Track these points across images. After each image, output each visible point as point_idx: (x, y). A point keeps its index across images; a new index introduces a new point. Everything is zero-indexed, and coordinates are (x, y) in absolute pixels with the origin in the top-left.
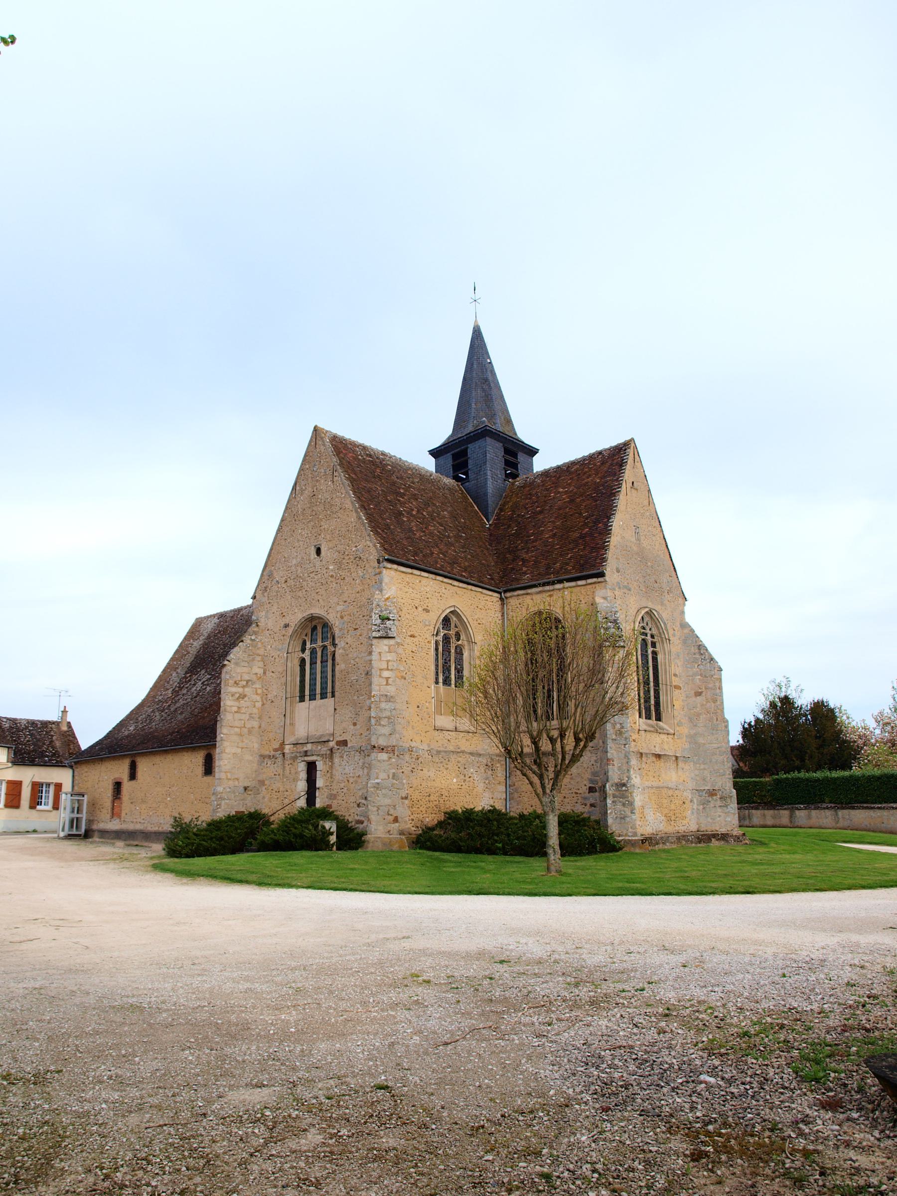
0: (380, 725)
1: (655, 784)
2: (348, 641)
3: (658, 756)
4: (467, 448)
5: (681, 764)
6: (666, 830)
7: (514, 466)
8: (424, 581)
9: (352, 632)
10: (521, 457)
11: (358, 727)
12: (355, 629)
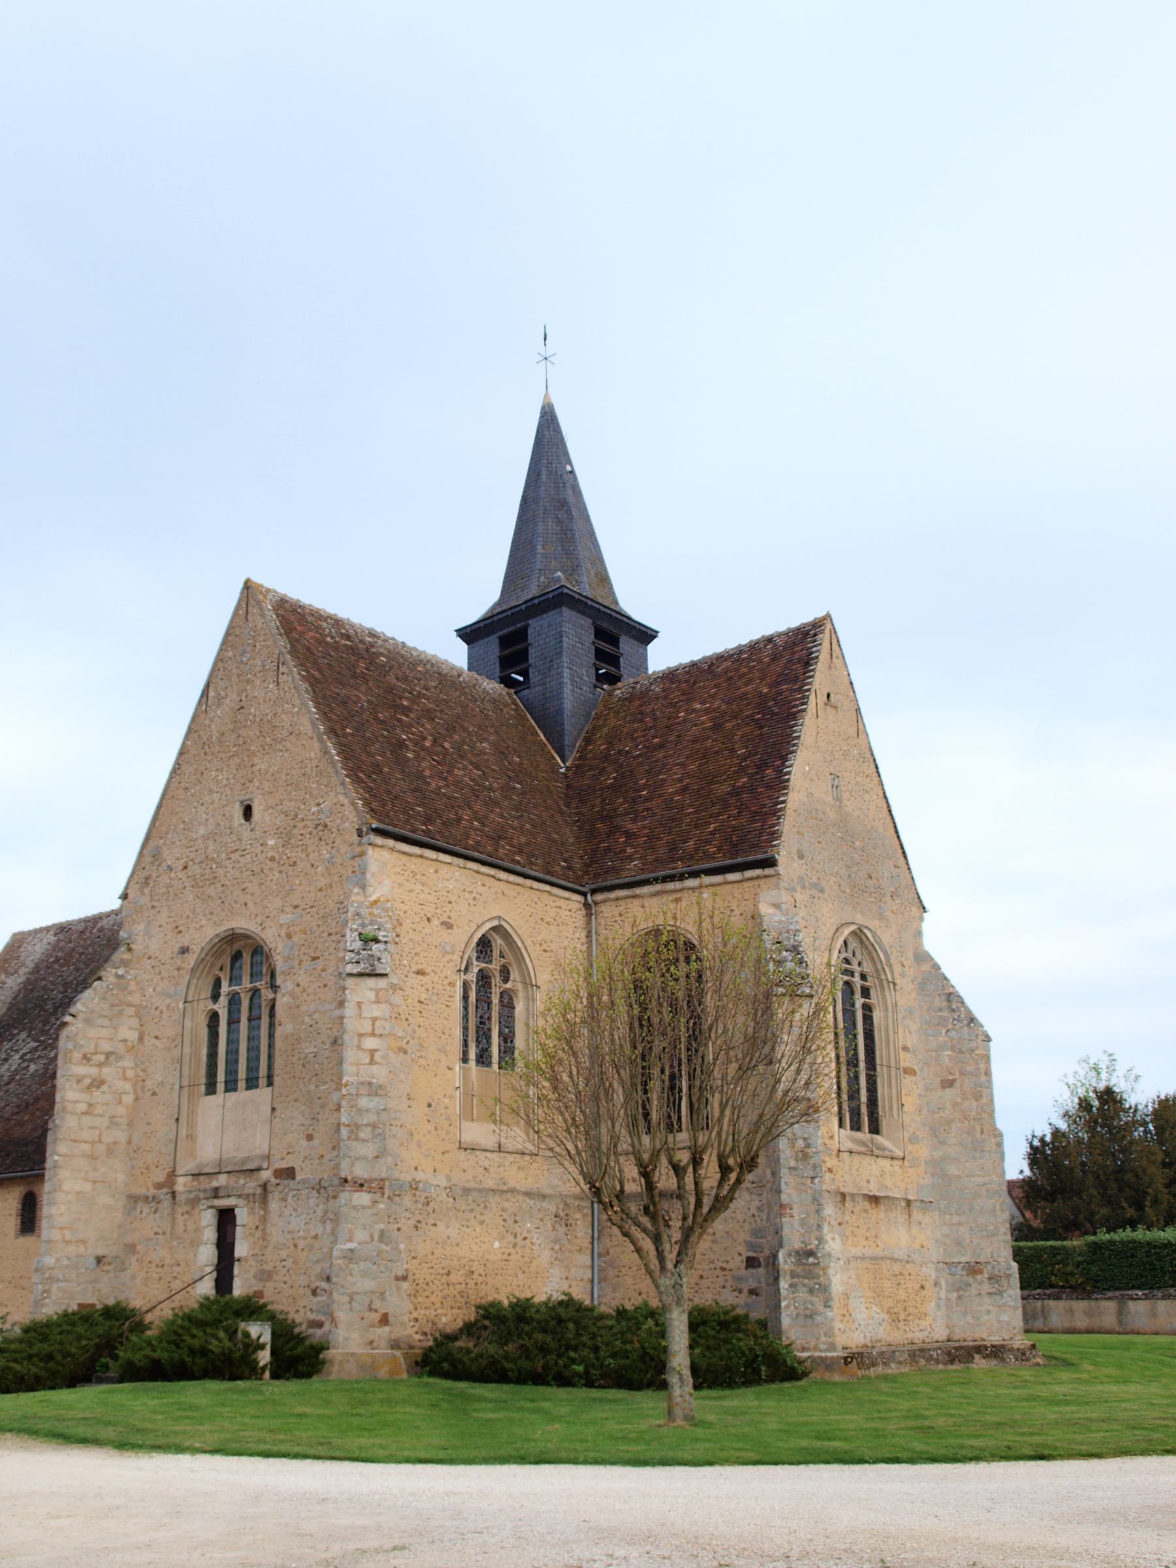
0: (357, 1139)
1: (868, 1252)
3: (875, 1200)
4: (526, 628)
5: (917, 1215)
6: (890, 1339)
7: (613, 660)
10: (626, 645)
11: (316, 1142)
12: (314, 959)
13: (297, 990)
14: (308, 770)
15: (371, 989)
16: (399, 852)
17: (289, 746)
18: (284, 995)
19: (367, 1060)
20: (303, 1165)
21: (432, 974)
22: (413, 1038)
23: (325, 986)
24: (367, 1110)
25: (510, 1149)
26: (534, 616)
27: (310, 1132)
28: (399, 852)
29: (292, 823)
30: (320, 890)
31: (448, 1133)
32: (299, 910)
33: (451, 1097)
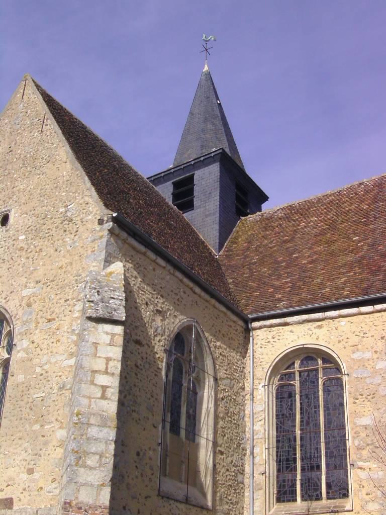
0: (85, 466)
2: (35, 338)
4: (194, 174)
8: (159, 271)
9: (43, 325)
11: (36, 475)
12: (49, 321)
13: (31, 346)
14: (60, 184)
15: (107, 333)
16: (130, 245)
17: (45, 170)
18: (19, 352)
19: (99, 395)
20: (22, 496)
21: (146, 346)
22: (130, 394)
23: (58, 341)
24: (96, 440)
25: (193, 503)
26: (199, 168)
27: (31, 466)
28: (130, 245)
29: (42, 222)
30: (61, 268)
31: (150, 480)
32: (40, 285)
33: (154, 450)
